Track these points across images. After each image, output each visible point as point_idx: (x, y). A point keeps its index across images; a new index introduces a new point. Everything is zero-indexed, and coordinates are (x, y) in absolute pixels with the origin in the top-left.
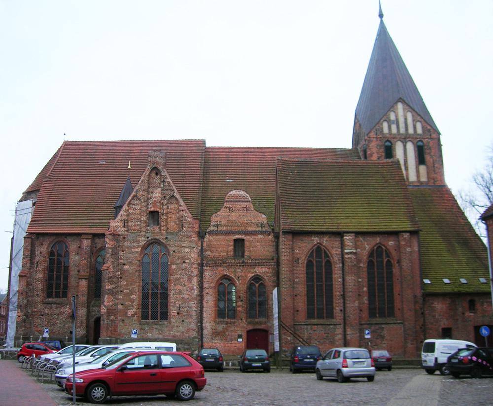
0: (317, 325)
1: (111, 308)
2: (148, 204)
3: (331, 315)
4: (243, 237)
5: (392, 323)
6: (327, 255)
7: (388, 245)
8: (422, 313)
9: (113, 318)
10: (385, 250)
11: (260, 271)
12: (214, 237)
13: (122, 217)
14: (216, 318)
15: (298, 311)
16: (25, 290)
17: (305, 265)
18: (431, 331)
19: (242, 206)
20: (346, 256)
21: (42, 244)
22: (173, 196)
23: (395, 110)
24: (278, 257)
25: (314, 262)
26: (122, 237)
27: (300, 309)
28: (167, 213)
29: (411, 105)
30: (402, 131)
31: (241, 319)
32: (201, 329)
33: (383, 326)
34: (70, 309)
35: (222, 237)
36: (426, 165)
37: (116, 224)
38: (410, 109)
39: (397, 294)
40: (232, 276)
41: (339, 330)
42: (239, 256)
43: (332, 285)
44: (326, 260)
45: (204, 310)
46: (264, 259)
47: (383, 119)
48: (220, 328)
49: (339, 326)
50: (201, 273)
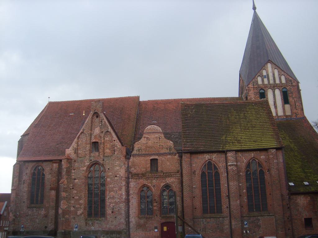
0: (210, 218)
1: (66, 210)
2: (91, 138)
3: (220, 211)
4: (156, 157)
5: (266, 216)
6: (215, 167)
7: (260, 158)
8: (288, 208)
9: (67, 216)
10: (258, 162)
11: (169, 180)
12: (137, 158)
13: (73, 147)
14: (139, 215)
15: (196, 208)
16: (15, 199)
17: (200, 176)
18: (296, 221)
19: (156, 136)
20: (229, 168)
21: (27, 168)
22: (108, 131)
23: (265, 69)
24: (182, 170)
25: (207, 173)
26: (73, 160)
27: (197, 207)
28: (104, 143)
29: (277, 64)
30: (272, 82)
31: (157, 215)
32: (128, 223)
33: (259, 218)
34: (45, 211)
35: (142, 158)
36: (290, 104)
37: (69, 151)
38: (277, 67)
39: (269, 194)
40: (150, 185)
41: (227, 221)
42: (155, 171)
43: (220, 189)
44: (215, 171)
45: (130, 209)
46: (172, 172)
47: (258, 75)
48: (142, 221)
49: (226, 218)
50: (128, 183)
